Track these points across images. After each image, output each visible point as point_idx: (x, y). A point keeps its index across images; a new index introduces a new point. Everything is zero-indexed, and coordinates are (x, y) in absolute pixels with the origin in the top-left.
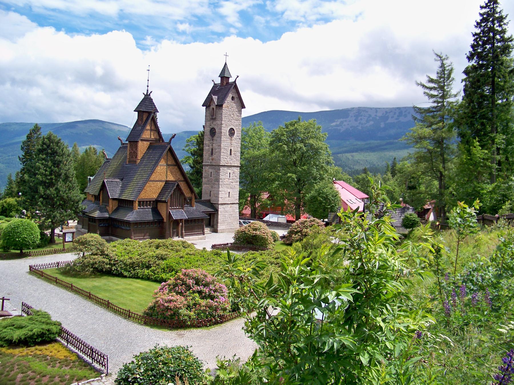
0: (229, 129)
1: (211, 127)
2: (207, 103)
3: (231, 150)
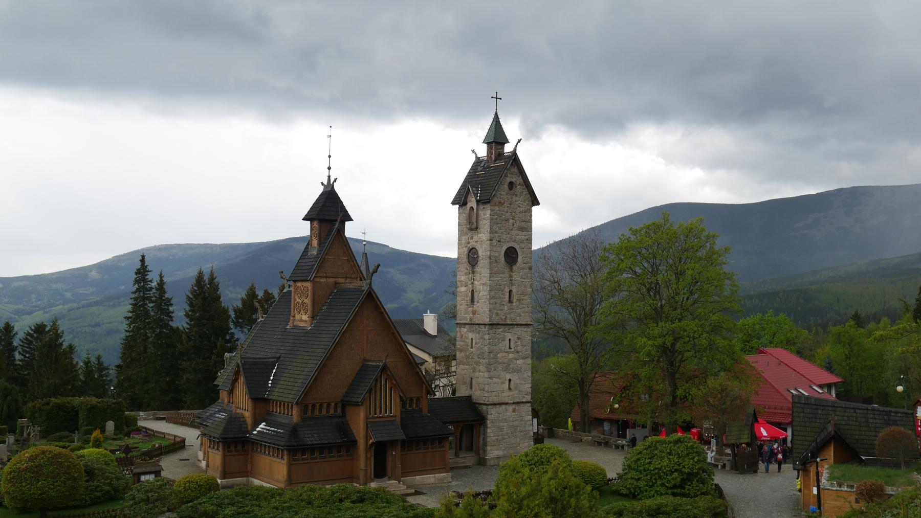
0: (505, 248)
2: (460, 200)
3: (510, 292)
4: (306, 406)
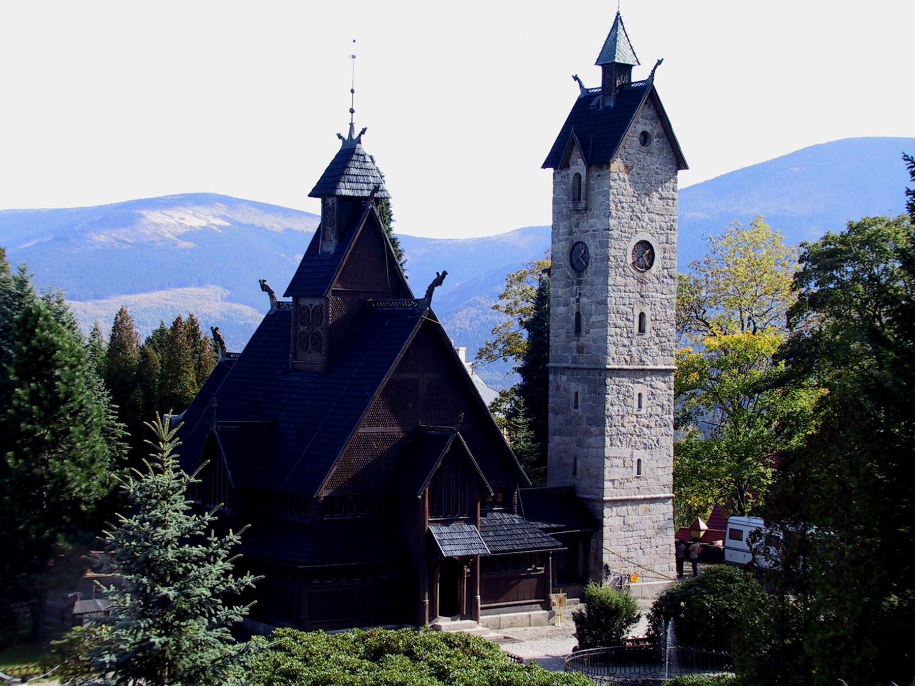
1: (577, 237)
2: (557, 159)
3: (642, 316)
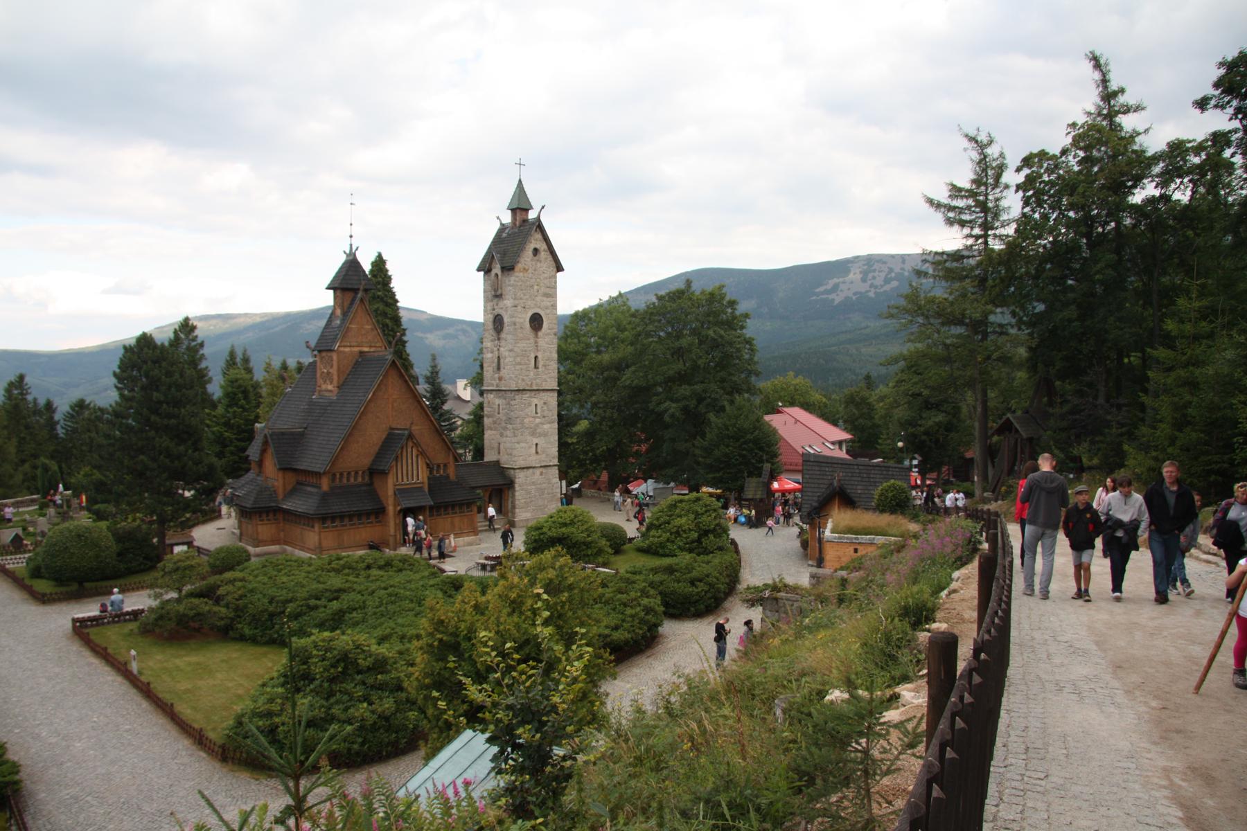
0: (530, 314)
1: (496, 312)
2: (485, 267)
3: (536, 358)
4: (334, 475)
